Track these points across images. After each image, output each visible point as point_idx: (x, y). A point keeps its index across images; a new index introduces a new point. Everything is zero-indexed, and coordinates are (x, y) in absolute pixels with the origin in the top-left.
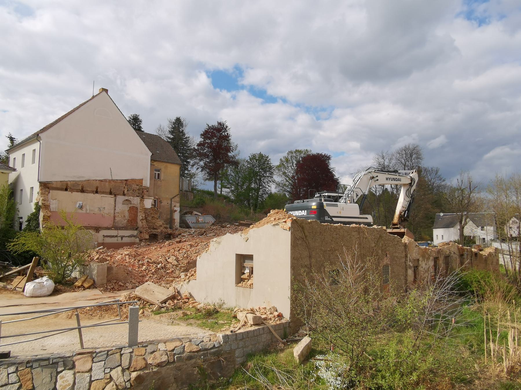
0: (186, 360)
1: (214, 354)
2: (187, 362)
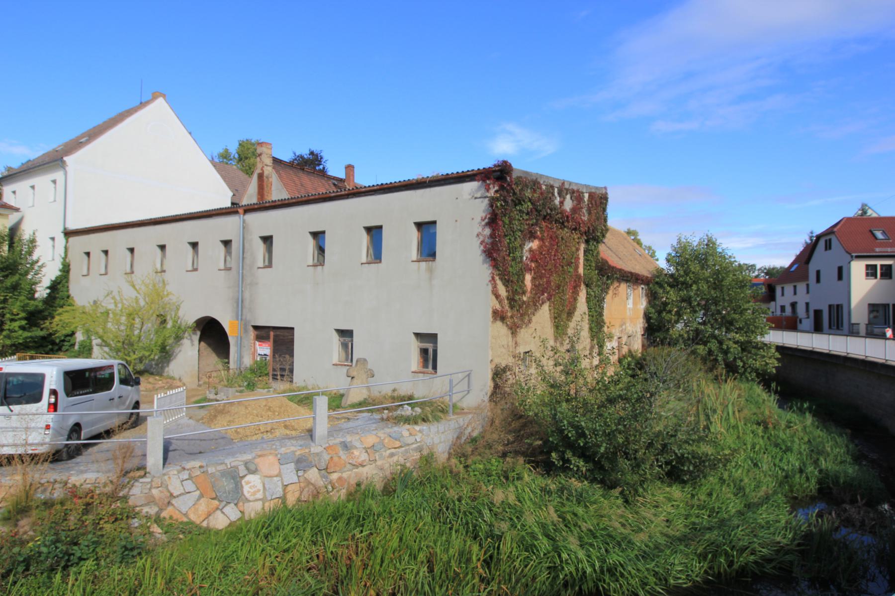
1: (415, 450)
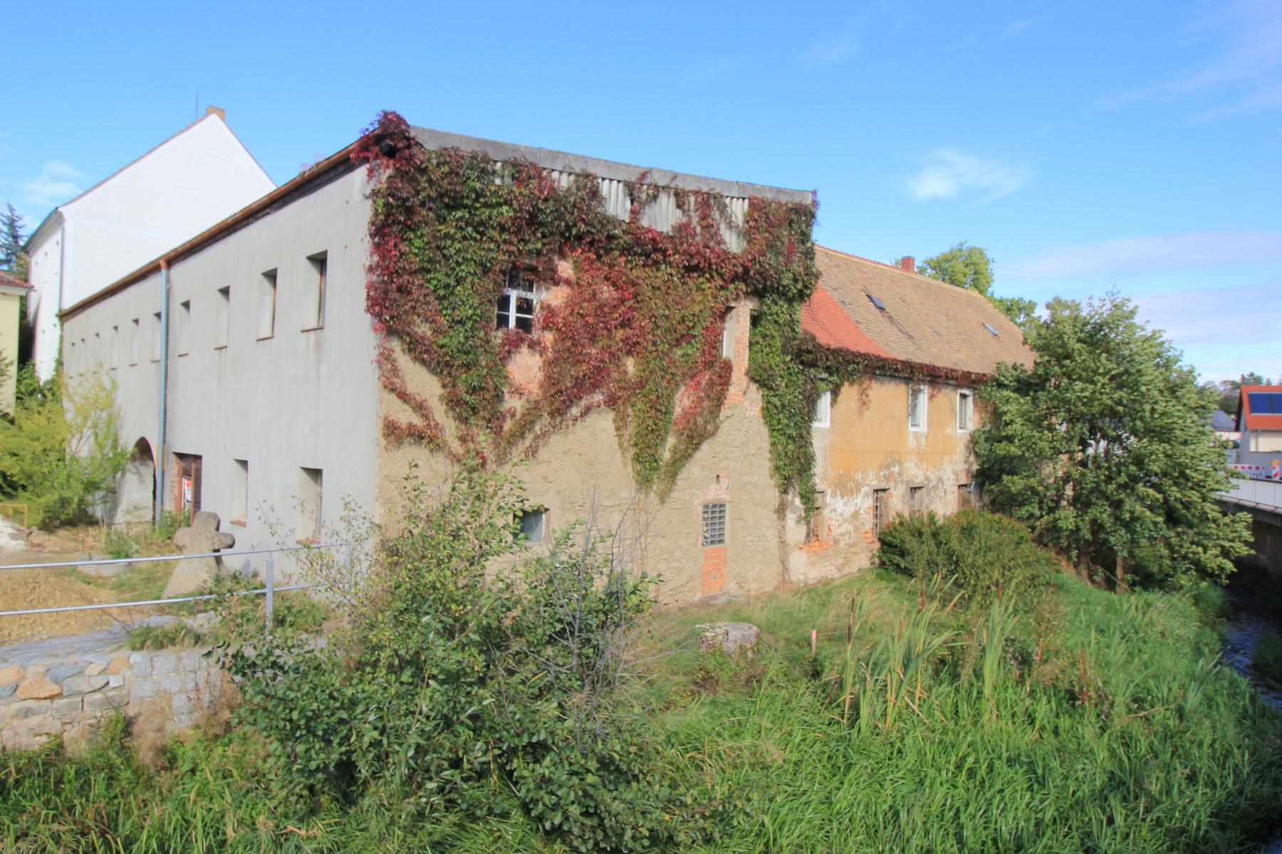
0: (13, 717)
2: (16, 723)
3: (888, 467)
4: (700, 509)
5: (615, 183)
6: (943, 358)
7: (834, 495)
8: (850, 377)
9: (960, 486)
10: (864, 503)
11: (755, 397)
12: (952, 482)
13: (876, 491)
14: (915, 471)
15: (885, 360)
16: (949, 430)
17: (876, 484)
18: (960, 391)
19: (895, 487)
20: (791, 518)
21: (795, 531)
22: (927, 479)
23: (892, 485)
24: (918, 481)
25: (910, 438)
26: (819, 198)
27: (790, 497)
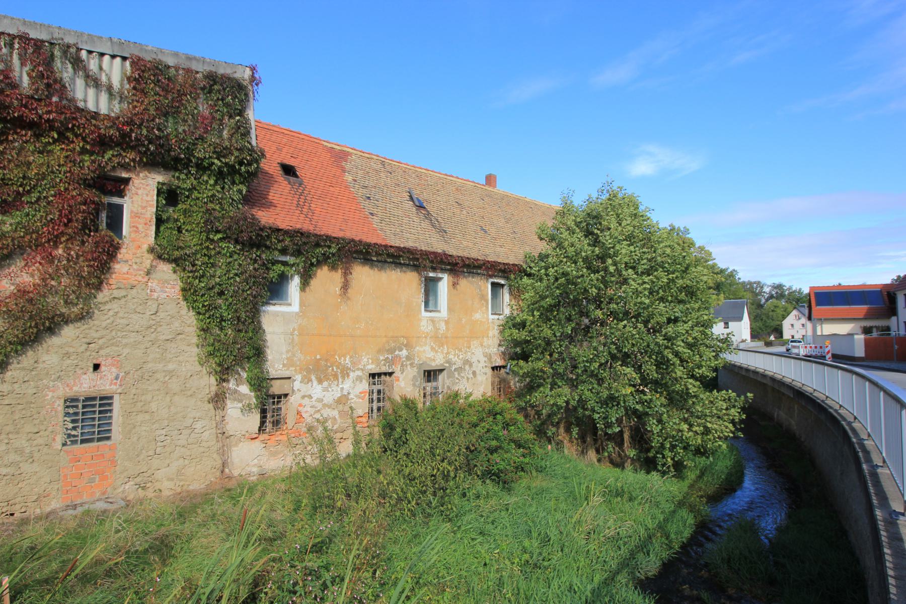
3: (391, 351)
4: (60, 406)
5: (118, 60)
6: (457, 248)
7: (307, 380)
8: (324, 260)
9: (493, 368)
10: (357, 389)
11: (167, 282)
12: (482, 364)
13: (373, 376)
14: (431, 355)
15: (369, 245)
16: (477, 316)
17: (373, 368)
18: (491, 280)
19: (402, 371)
20: (233, 409)
21: (240, 417)
22: (448, 362)
23: (397, 369)
24: (434, 365)
25: (424, 323)
26: (260, 74)
27: (232, 385)
